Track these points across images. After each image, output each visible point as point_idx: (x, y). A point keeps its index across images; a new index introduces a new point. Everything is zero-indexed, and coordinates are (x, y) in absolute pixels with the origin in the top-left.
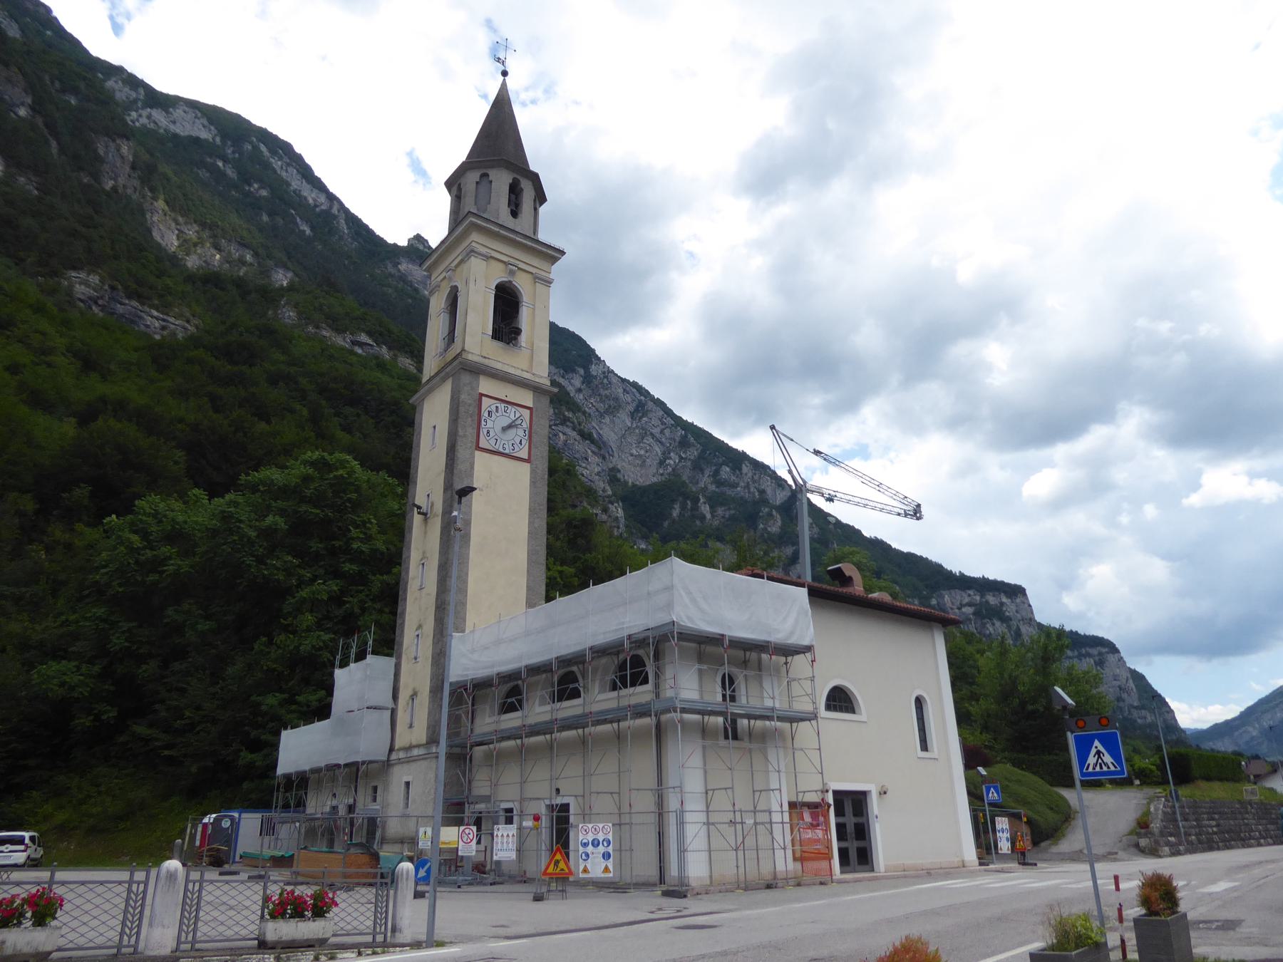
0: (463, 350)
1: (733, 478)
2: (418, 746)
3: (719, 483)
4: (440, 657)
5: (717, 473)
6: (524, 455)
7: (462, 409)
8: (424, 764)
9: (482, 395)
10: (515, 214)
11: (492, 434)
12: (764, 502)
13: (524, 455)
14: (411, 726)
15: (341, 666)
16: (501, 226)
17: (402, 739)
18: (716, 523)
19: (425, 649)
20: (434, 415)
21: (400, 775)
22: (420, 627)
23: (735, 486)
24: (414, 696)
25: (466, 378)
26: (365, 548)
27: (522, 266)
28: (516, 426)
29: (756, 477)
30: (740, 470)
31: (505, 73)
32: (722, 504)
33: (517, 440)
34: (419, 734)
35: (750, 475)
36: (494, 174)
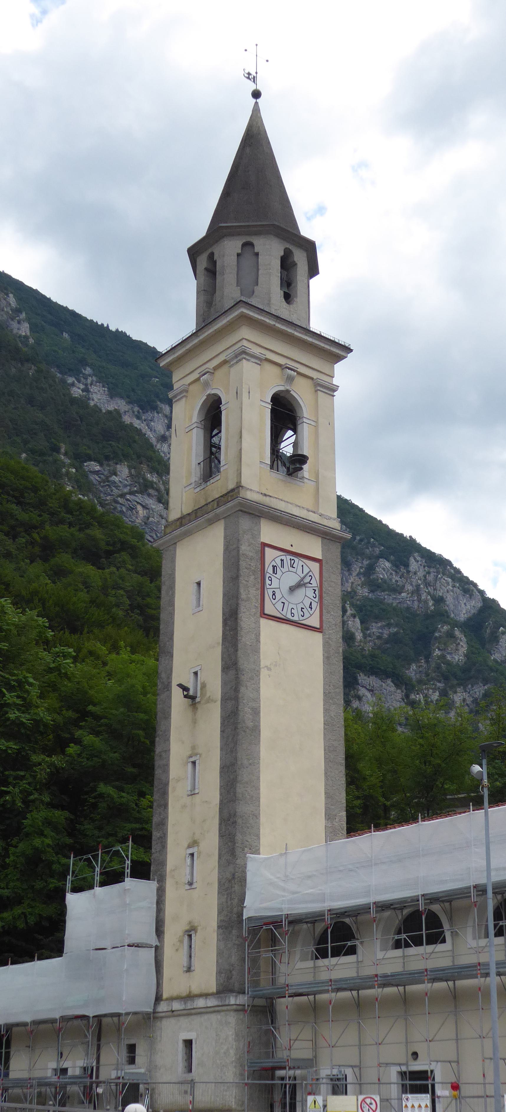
0: (239, 486)
1: (395, 578)
2: (205, 995)
3: (375, 586)
4: (232, 884)
5: (370, 570)
6: (315, 622)
7: (243, 564)
8: (214, 1018)
9: (264, 545)
10: (288, 297)
11: (278, 596)
12: (441, 614)
13: (315, 622)
14: (189, 970)
15: (76, 890)
16: (278, 318)
17: (175, 983)
18: (369, 647)
19: (208, 870)
20: (196, 569)
21: (172, 1034)
22: (195, 843)
23: (397, 590)
24: (190, 933)
25: (245, 523)
26: (25, 718)
27: (302, 370)
28: (304, 585)
29: (430, 578)
30: (407, 565)
31: (256, 94)
32: (378, 618)
33: (304, 603)
34: (205, 977)
35: (421, 574)
36: (261, 244)
